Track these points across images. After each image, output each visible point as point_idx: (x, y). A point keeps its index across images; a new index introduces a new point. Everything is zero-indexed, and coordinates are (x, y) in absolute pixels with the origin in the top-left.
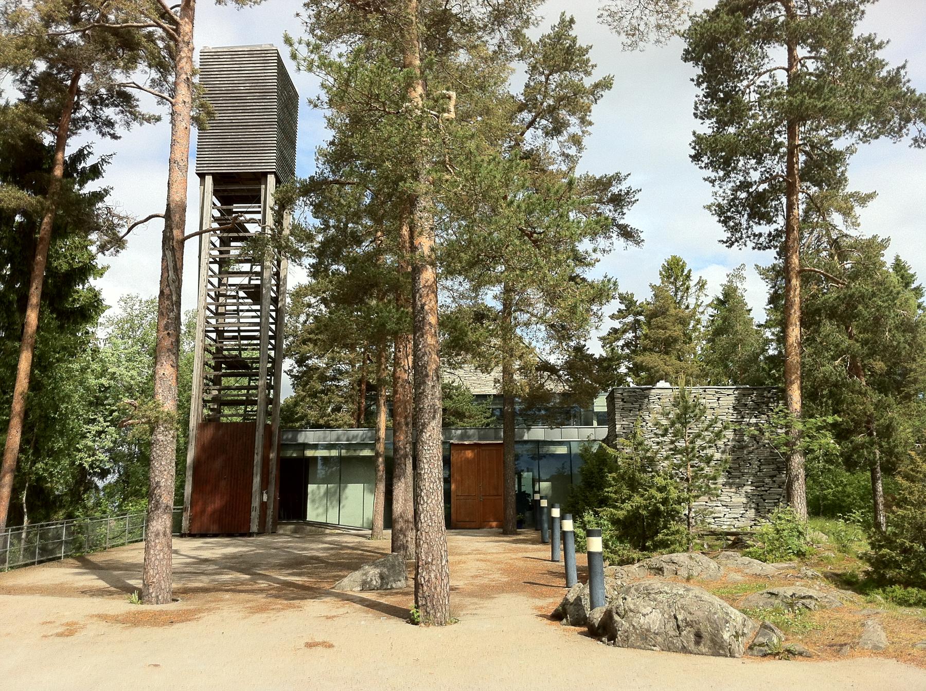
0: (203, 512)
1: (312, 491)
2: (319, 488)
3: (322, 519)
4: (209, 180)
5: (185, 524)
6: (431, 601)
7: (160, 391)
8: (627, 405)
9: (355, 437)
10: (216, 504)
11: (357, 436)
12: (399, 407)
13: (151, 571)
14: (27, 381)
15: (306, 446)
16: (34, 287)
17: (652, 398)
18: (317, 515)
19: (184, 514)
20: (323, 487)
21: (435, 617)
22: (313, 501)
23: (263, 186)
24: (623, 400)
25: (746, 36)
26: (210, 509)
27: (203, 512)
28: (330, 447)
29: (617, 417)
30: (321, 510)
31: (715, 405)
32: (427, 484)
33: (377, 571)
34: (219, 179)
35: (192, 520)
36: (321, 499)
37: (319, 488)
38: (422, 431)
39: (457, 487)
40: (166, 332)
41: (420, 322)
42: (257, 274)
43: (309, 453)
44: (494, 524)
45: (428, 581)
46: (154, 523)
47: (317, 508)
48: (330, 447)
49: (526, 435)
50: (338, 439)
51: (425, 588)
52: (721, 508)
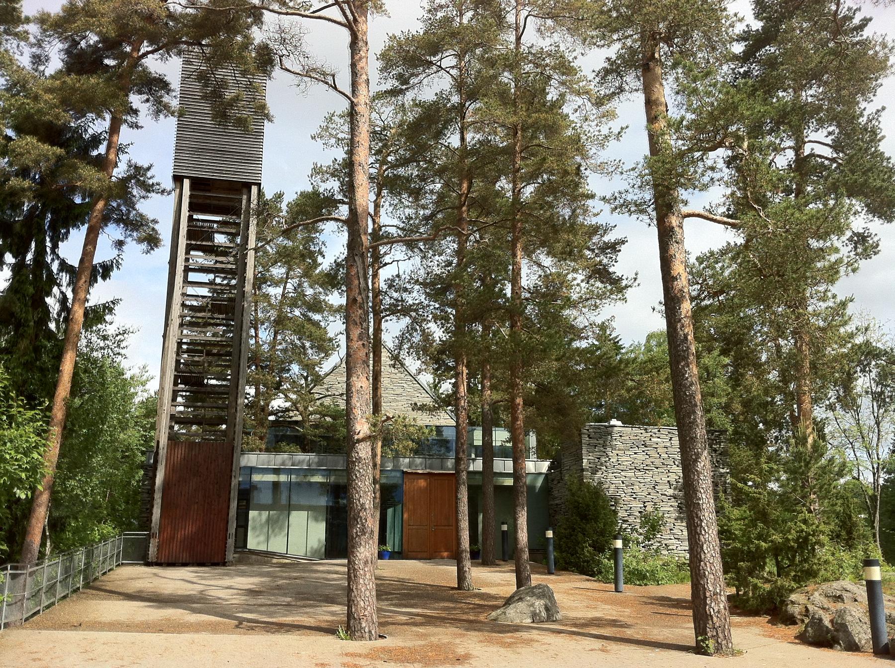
0: (172, 538)
1: (253, 518)
2: (260, 515)
3: (263, 548)
4: (187, 183)
5: (152, 550)
6: (723, 632)
7: (358, 405)
8: (592, 441)
9: (300, 463)
10: (189, 529)
11: (303, 461)
12: (520, 434)
13: (362, 603)
14: (69, 385)
15: (252, 470)
16: (83, 280)
17: (615, 436)
18: (258, 543)
19: (152, 540)
20: (265, 514)
21: (727, 647)
22: (254, 528)
23: (245, 197)
24: (589, 436)
25: (742, 118)
26: (179, 535)
27: (172, 538)
28: (276, 471)
29: (584, 452)
30: (262, 538)
31: (669, 444)
32: (706, 514)
33: (542, 602)
34: (196, 184)
35: (159, 548)
36: (262, 526)
37: (260, 515)
38: (696, 461)
39: (409, 516)
40: (360, 343)
41: (683, 351)
42: (234, 287)
43: (256, 478)
44: (445, 554)
45: (718, 612)
46: (362, 549)
47: (258, 536)
48: (276, 471)
49: (472, 465)
50: (283, 464)
51: (715, 619)
52: (674, 541)
